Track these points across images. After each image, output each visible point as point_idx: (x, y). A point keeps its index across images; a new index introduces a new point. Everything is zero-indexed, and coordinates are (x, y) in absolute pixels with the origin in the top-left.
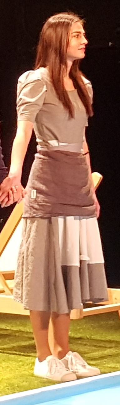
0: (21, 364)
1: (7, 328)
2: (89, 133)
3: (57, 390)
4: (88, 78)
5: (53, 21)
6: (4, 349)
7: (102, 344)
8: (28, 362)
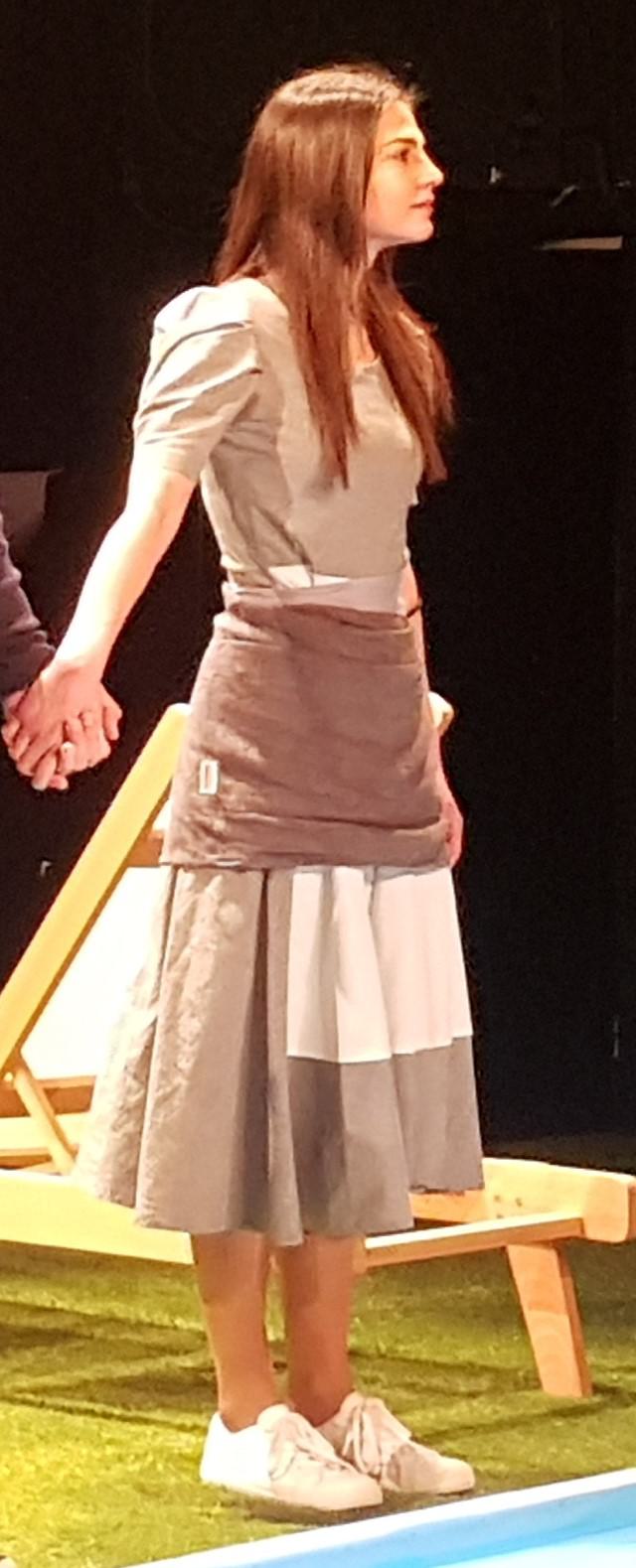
0: (114, 1455)
1: (59, 1305)
2: (432, 531)
4: (425, 315)
5: (299, 100)
6: (45, 1390)
7: (437, 1381)
8: (141, 1447)
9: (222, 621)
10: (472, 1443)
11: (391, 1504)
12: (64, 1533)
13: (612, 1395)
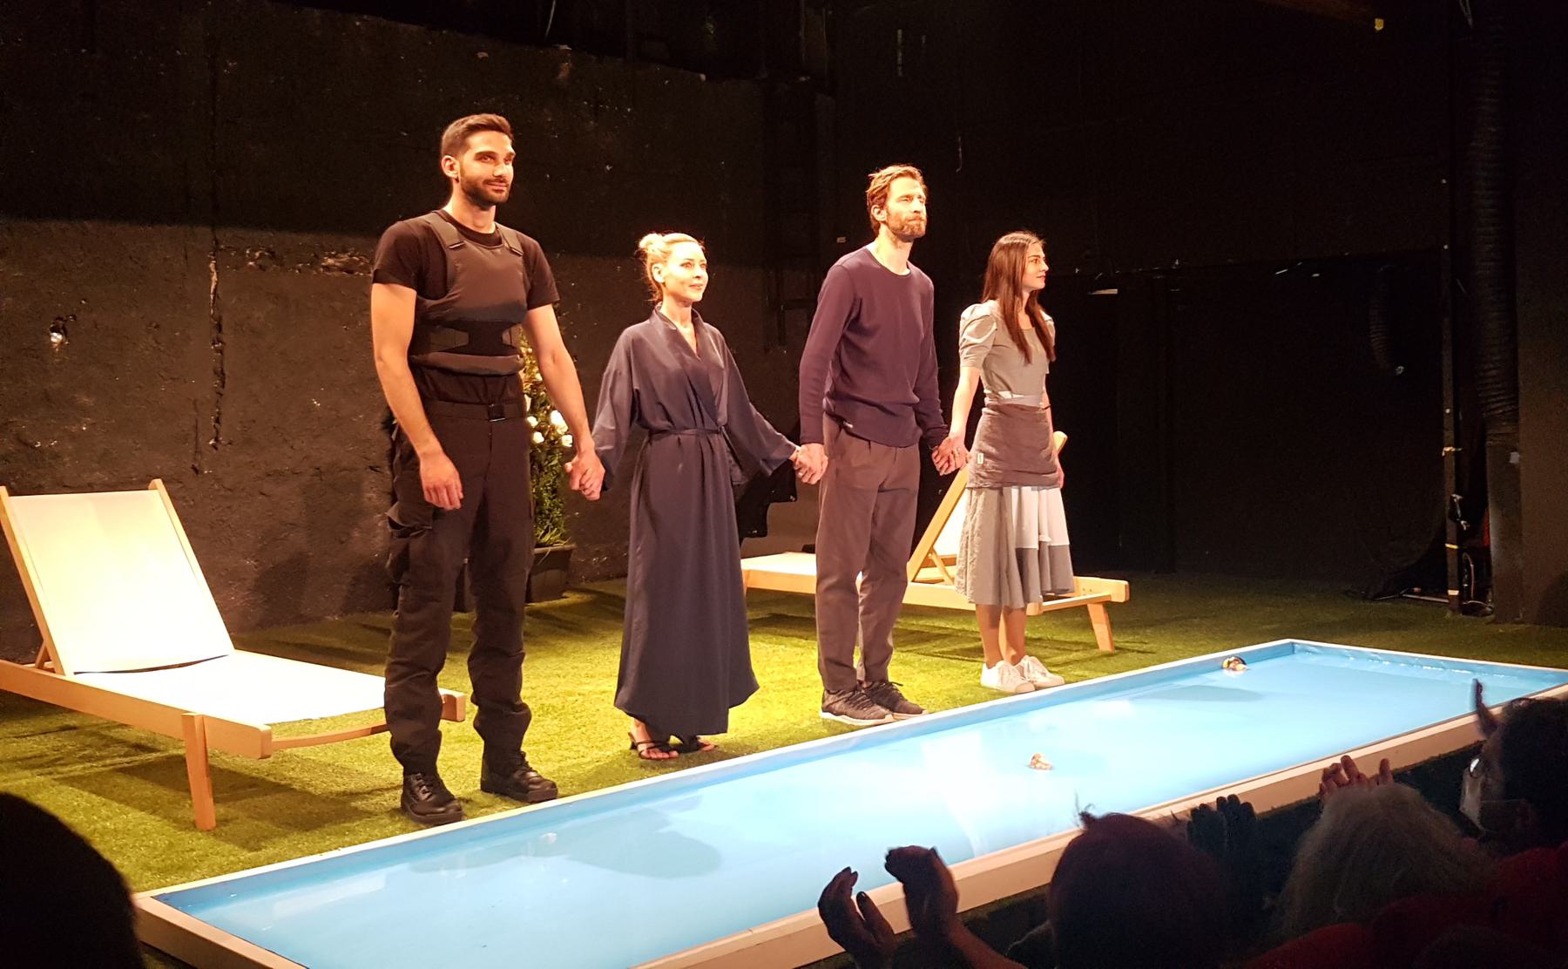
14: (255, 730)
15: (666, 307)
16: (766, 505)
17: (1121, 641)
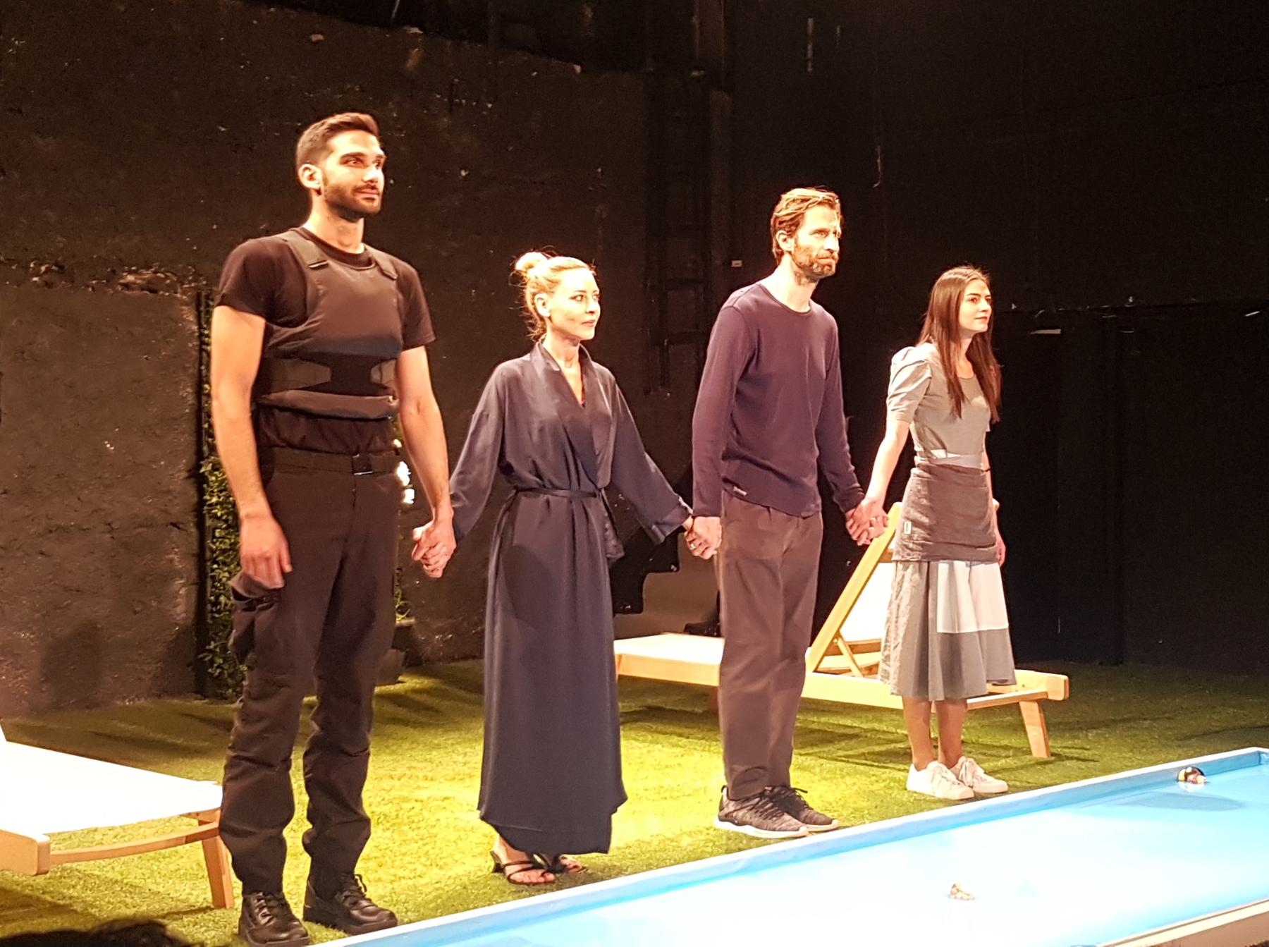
2: (993, 443)
3: (927, 821)
7: (994, 752)
9: (914, 471)
10: (1006, 775)
11: (978, 797)
12: (856, 810)
13: (1059, 757)
14: (32, 841)
15: (550, 342)
16: (645, 575)
17: (1058, 746)
